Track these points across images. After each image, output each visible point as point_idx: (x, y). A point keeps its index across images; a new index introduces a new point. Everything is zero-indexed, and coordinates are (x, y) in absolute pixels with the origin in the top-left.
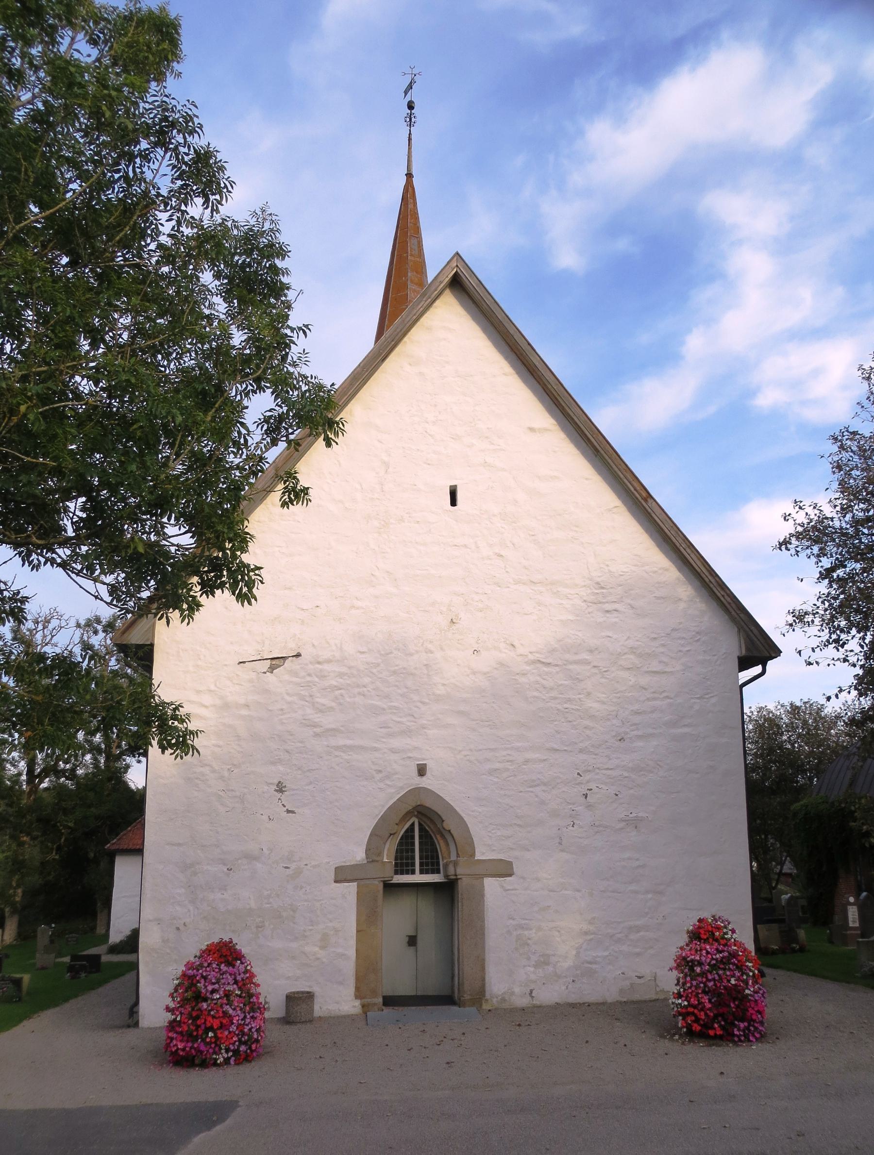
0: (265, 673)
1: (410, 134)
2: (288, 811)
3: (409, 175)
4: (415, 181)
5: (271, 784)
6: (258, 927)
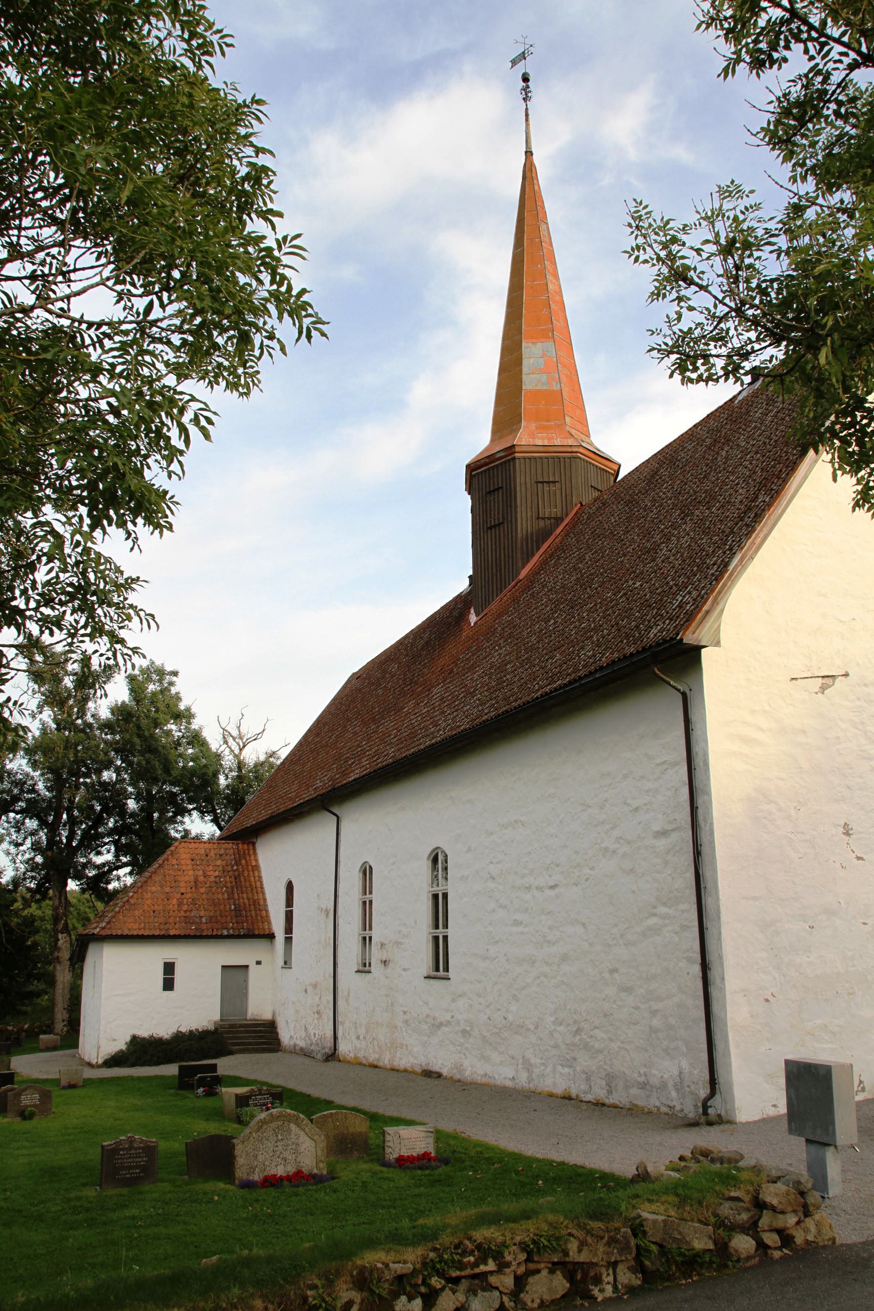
0: (816, 693)
1: (527, 109)
2: (859, 858)
3: (529, 153)
4: (536, 159)
5: (839, 825)
6: (849, 994)
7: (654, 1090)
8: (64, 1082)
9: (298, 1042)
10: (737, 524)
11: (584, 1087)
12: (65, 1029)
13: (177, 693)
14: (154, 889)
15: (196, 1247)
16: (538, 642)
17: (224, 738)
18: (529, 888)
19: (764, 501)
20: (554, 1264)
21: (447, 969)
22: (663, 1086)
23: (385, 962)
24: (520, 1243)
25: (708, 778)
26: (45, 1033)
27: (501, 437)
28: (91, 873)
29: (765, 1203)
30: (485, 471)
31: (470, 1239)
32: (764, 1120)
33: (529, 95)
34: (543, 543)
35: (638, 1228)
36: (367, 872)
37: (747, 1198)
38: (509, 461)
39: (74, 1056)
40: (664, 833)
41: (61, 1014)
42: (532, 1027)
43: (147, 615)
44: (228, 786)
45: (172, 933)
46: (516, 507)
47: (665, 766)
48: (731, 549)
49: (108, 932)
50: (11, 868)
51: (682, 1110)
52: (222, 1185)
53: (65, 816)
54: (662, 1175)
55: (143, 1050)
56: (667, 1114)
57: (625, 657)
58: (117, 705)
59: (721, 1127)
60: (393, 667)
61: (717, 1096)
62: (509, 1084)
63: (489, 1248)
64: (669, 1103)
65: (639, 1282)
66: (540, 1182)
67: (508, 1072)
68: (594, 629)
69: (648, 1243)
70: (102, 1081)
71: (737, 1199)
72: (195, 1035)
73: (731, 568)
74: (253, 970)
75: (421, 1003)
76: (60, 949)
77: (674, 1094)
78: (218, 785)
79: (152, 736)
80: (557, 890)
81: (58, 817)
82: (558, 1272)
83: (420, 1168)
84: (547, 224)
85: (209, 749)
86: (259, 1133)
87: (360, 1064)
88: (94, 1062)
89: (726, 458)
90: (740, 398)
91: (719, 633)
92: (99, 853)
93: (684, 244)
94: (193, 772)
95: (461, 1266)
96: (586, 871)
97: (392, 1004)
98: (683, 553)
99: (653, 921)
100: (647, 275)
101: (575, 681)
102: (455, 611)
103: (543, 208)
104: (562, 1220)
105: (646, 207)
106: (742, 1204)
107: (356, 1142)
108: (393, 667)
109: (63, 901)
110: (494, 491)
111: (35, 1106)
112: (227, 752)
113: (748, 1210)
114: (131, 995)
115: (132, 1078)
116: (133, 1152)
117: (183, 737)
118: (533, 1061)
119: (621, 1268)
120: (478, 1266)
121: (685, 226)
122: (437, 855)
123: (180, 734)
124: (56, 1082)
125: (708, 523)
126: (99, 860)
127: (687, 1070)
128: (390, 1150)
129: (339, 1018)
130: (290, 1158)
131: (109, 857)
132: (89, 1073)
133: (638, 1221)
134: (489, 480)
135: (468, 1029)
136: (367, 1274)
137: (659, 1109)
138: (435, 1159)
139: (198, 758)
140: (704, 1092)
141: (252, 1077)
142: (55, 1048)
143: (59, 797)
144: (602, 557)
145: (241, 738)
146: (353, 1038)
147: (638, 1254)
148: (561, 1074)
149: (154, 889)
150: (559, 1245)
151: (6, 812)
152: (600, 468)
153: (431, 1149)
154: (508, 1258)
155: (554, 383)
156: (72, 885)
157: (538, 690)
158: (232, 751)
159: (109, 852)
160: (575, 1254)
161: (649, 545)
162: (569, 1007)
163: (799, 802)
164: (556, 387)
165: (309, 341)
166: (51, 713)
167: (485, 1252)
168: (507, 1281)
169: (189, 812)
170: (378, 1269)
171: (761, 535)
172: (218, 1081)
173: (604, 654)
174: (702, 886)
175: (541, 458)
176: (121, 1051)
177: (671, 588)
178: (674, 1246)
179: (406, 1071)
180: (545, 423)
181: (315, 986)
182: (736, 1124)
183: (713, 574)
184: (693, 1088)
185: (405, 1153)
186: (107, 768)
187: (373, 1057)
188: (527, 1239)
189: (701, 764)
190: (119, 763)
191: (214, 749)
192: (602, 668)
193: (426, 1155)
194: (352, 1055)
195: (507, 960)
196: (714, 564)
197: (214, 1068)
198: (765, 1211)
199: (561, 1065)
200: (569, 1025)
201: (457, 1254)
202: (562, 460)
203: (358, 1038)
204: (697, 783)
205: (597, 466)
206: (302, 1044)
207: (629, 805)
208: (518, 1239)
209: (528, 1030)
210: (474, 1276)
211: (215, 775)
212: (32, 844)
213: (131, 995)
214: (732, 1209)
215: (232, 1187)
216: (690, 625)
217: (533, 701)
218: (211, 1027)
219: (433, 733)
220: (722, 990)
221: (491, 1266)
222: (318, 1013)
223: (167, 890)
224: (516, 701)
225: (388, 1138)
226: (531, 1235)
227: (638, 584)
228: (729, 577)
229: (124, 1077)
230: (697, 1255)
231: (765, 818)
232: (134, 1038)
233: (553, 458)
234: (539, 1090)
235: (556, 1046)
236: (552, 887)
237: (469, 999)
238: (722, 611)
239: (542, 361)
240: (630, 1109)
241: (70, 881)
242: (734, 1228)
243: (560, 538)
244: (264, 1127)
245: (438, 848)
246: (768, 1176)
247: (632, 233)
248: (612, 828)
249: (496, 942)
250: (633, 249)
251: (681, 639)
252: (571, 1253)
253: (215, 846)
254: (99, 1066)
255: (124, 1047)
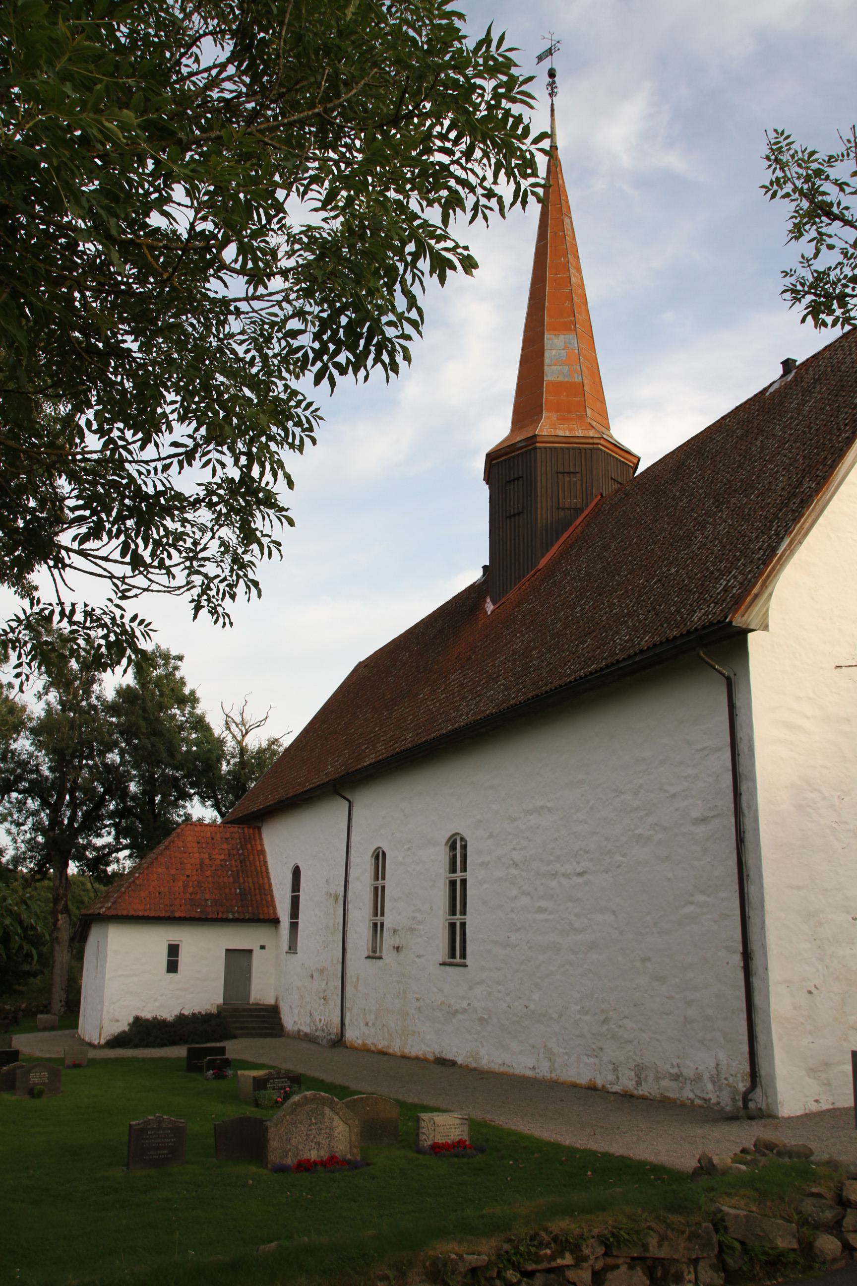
1: (552, 105)
7: (688, 1082)
8: (68, 1062)
9: (302, 1028)
10: (781, 510)
11: (611, 1078)
12: (63, 1009)
13: (182, 678)
14: (160, 870)
15: (239, 1232)
16: (565, 628)
17: (227, 723)
18: (554, 875)
19: (810, 487)
20: (633, 1259)
21: (464, 956)
22: (698, 1078)
23: (398, 948)
24: (598, 1236)
25: (753, 764)
26: (42, 1012)
27: (521, 428)
28: (90, 854)
29: (849, 1201)
30: (505, 460)
31: (546, 1230)
32: (806, 1115)
33: (555, 90)
34: (563, 533)
35: (719, 1223)
36: (379, 857)
37: (829, 1195)
38: (530, 451)
39: (74, 1036)
40: (703, 820)
41: (58, 996)
42: (555, 1016)
43: (272, 542)
44: (229, 772)
45: (177, 915)
46: (536, 496)
47: (706, 752)
48: (777, 534)
49: (114, 912)
50: (11, 848)
51: (719, 1103)
52: (253, 1169)
53: (68, 797)
54: (731, 1168)
55: (145, 1032)
56: (701, 1107)
57: (668, 640)
58: (121, 688)
59: (763, 1121)
60: (404, 656)
61: (758, 1090)
62: (529, 1073)
63: (567, 1240)
64: (704, 1095)
65: (722, 1282)
66: (589, 1173)
67: (531, 1063)
68: (627, 614)
69: (731, 1240)
70: (106, 1061)
71: (819, 1195)
72: (198, 1018)
73: (780, 552)
74: (257, 954)
75: (436, 990)
76: (59, 929)
77: (710, 1086)
78: (221, 770)
79: (158, 719)
80: (586, 877)
81: (61, 798)
82: (638, 1268)
83: (457, 1156)
84: (570, 218)
85: (212, 734)
86: (293, 1116)
87: (369, 1051)
88: (96, 1043)
89: (762, 448)
90: (771, 390)
91: (767, 616)
92: (99, 835)
93: (827, 178)
94: (196, 756)
95: (538, 1259)
96: (618, 858)
97: (405, 991)
98: (722, 539)
99: (690, 909)
100: (785, 210)
101: (613, 664)
102: (470, 599)
103: (567, 202)
104: (640, 1212)
105: (788, 137)
106: (825, 1201)
107: (389, 1128)
108: (404, 656)
109: (64, 881)
110: (514, 480)
111: (43, 1084)
112: (229, 738)
113: (831, 1207)
114: (133, 976)
115: (136, 1059)
116: (161, 1132)
117: (186, 721)
118: (555, 1051)
119: (702, 1265)
120: (555, 1260)
121: (831, 157)
122: (455, 842)
123: (183, 719)
124: (61, 1061)
125: (747, 510)
126: (99, 842)
127: (725, 1062)
128: (425, 1137)
129: (347, 1004)
130: (323, 1142)
131: (110, 839)
132: (92, 1054)
133: (719, 1216)
134: (508, 470)
135: (486, 1017)
136: (440, 1266)
137: (692, 1101)
138: (471, 1147)
139: (202, 742)
140: (742, 1086)
141: (261, 1061)
142: (52, 1028)
143: (62, 778)
144: (630, 545)
145: (245, 726)
146: (362, 1025)
147: (721, 1251)
148: (586, 1064)
149: (160, 870)
150: (639, 1239)
151: (9, 791)
152: (620, 461)
153: (465, 1137)
154: (586, 1251)
155: (576, 375)
156: (73, 868)
157: (570, 675)
158: (234, 737)
159: (109, 833)
160: (655, 1250)
161: (681, 532)
162: (596, 996)
163: (843, 791)
164: (577, 379)
165: (524, 208)
166: (57, 694)
167: (562, 1244)
168: (584, 1276)
169: (190, 797)
170: (452, 1260)
171: (810, 521)
172: (227, 1063)
173: (642, 639)
174: (745, 874)
175: (562, 448)
176: (124, 1032)
177: (712, 573)
178: (757, 1243)
179: (417, 1058)
180: (566, 415)
181: (322, 971)
182: (778, 1118)
183: (759, 559)
184: (731, 1080)
185: (440, 1139)
186: (111, 750)
187: (382, 1044)
188: (606, 1232)
189: (746, 749)
190: (123, 745)
191: (216, 736)
192: (642, 651)
193: (461, 1143)
194: (360, 1042)
195: (530, 948)
196: (760, 549)
197: (222, 1050)
198: (849, 1210)
199: (587, 1055)
200: (596, 1014)
201: (534, 1246)
202: (583, 452)
203: (367, 1024)
204: (742, 769)
205: (617, 459)
206: (306, 1029)
207: (666, 791)
208: (596, 1231)
209: (551, 1018)
210: (549, 1271)
211: (219, 761)
212: (34, 825)
213: (133, 976)
214: (815, 1206)
215: (265, 1171)
216: (739, 608)
217: (566, 685)
218: (214, 1010)
219: (454, 718)
220: (766, 980)
221: (568, 1260)
222: (324, 999)
223: (173, 872)
224: (546, 685)
225: (423, 1124)
226: (610, 1228)
227: (673, 570)
228: (780, 558)
229: (128, 1058)
230: (781, 1255)
231: (809, 806)
232: (137, 1019)
233: (574, 449)
234: (562, 1079)
235: (581, 1036)
236: (580, 874)
237: (488, 986)
238: (771, 595)
239: (563, 353)
240: (660, 1101)
241: (70, 862)
242: (817, 1226)
243: (580, 528)
244: (298, 1110)
245: (457, 834)
246: (848, 1172)
247: (770, 166)
248: (647, 815)
249: (518, 930)
250: (772, 183)
251: (731, 622)
252: (651, 1248)
253: (221, 829)
254: (100, 1047)
255: (127, 1029)
